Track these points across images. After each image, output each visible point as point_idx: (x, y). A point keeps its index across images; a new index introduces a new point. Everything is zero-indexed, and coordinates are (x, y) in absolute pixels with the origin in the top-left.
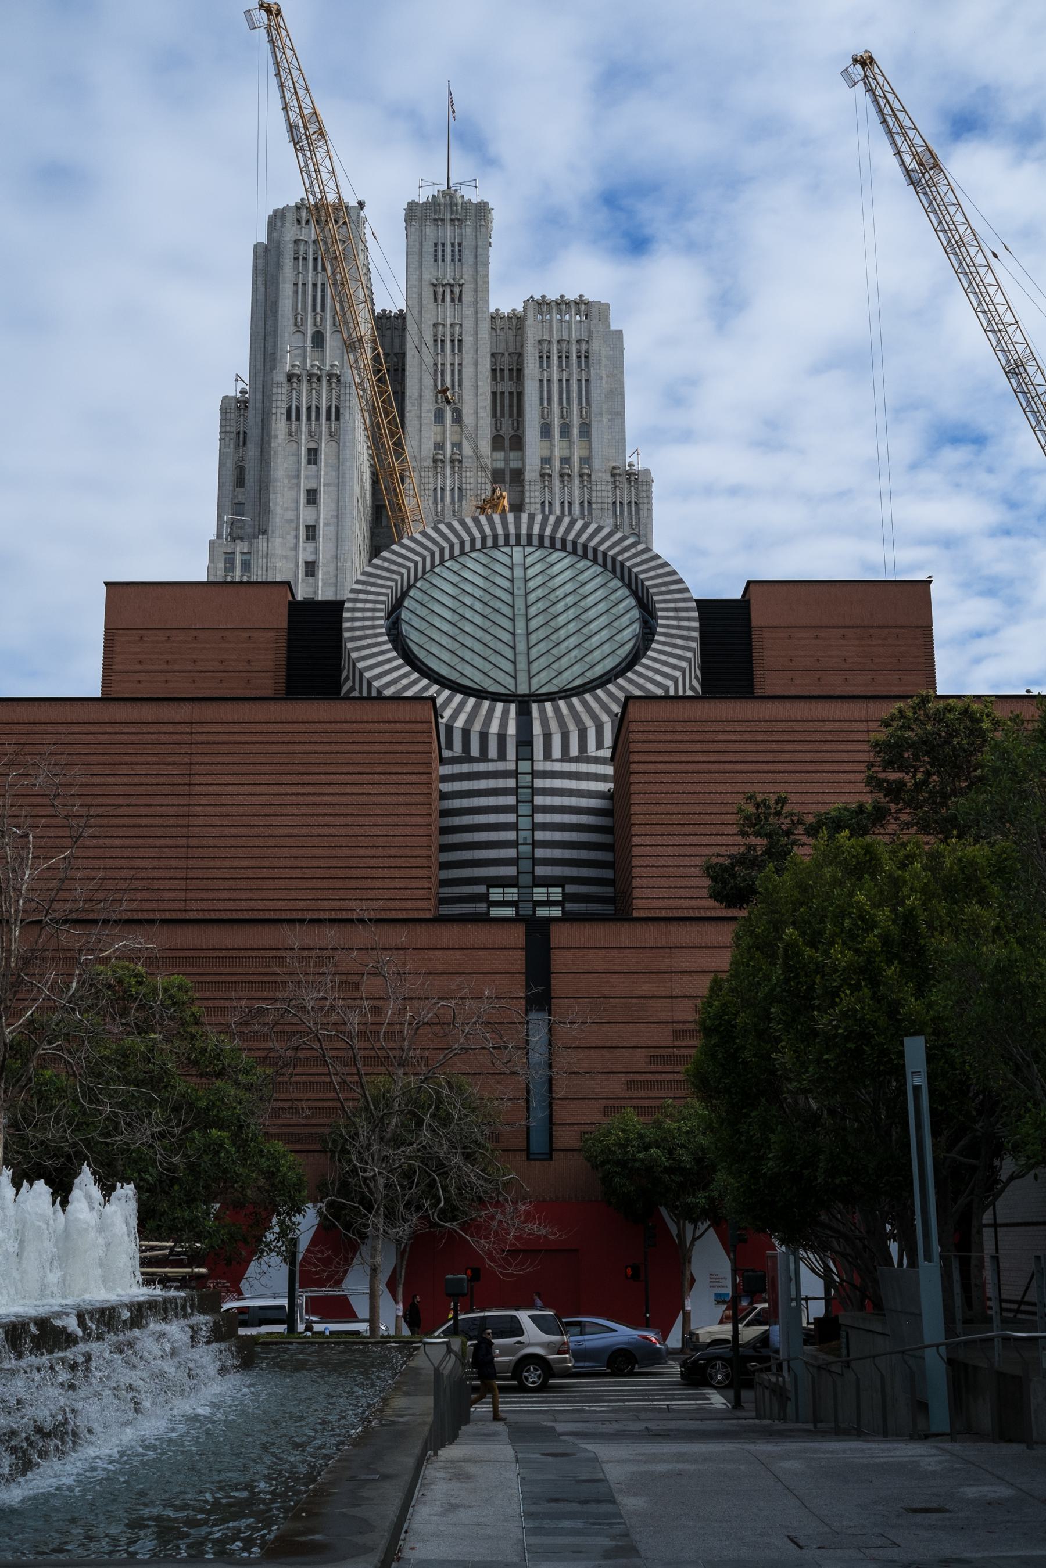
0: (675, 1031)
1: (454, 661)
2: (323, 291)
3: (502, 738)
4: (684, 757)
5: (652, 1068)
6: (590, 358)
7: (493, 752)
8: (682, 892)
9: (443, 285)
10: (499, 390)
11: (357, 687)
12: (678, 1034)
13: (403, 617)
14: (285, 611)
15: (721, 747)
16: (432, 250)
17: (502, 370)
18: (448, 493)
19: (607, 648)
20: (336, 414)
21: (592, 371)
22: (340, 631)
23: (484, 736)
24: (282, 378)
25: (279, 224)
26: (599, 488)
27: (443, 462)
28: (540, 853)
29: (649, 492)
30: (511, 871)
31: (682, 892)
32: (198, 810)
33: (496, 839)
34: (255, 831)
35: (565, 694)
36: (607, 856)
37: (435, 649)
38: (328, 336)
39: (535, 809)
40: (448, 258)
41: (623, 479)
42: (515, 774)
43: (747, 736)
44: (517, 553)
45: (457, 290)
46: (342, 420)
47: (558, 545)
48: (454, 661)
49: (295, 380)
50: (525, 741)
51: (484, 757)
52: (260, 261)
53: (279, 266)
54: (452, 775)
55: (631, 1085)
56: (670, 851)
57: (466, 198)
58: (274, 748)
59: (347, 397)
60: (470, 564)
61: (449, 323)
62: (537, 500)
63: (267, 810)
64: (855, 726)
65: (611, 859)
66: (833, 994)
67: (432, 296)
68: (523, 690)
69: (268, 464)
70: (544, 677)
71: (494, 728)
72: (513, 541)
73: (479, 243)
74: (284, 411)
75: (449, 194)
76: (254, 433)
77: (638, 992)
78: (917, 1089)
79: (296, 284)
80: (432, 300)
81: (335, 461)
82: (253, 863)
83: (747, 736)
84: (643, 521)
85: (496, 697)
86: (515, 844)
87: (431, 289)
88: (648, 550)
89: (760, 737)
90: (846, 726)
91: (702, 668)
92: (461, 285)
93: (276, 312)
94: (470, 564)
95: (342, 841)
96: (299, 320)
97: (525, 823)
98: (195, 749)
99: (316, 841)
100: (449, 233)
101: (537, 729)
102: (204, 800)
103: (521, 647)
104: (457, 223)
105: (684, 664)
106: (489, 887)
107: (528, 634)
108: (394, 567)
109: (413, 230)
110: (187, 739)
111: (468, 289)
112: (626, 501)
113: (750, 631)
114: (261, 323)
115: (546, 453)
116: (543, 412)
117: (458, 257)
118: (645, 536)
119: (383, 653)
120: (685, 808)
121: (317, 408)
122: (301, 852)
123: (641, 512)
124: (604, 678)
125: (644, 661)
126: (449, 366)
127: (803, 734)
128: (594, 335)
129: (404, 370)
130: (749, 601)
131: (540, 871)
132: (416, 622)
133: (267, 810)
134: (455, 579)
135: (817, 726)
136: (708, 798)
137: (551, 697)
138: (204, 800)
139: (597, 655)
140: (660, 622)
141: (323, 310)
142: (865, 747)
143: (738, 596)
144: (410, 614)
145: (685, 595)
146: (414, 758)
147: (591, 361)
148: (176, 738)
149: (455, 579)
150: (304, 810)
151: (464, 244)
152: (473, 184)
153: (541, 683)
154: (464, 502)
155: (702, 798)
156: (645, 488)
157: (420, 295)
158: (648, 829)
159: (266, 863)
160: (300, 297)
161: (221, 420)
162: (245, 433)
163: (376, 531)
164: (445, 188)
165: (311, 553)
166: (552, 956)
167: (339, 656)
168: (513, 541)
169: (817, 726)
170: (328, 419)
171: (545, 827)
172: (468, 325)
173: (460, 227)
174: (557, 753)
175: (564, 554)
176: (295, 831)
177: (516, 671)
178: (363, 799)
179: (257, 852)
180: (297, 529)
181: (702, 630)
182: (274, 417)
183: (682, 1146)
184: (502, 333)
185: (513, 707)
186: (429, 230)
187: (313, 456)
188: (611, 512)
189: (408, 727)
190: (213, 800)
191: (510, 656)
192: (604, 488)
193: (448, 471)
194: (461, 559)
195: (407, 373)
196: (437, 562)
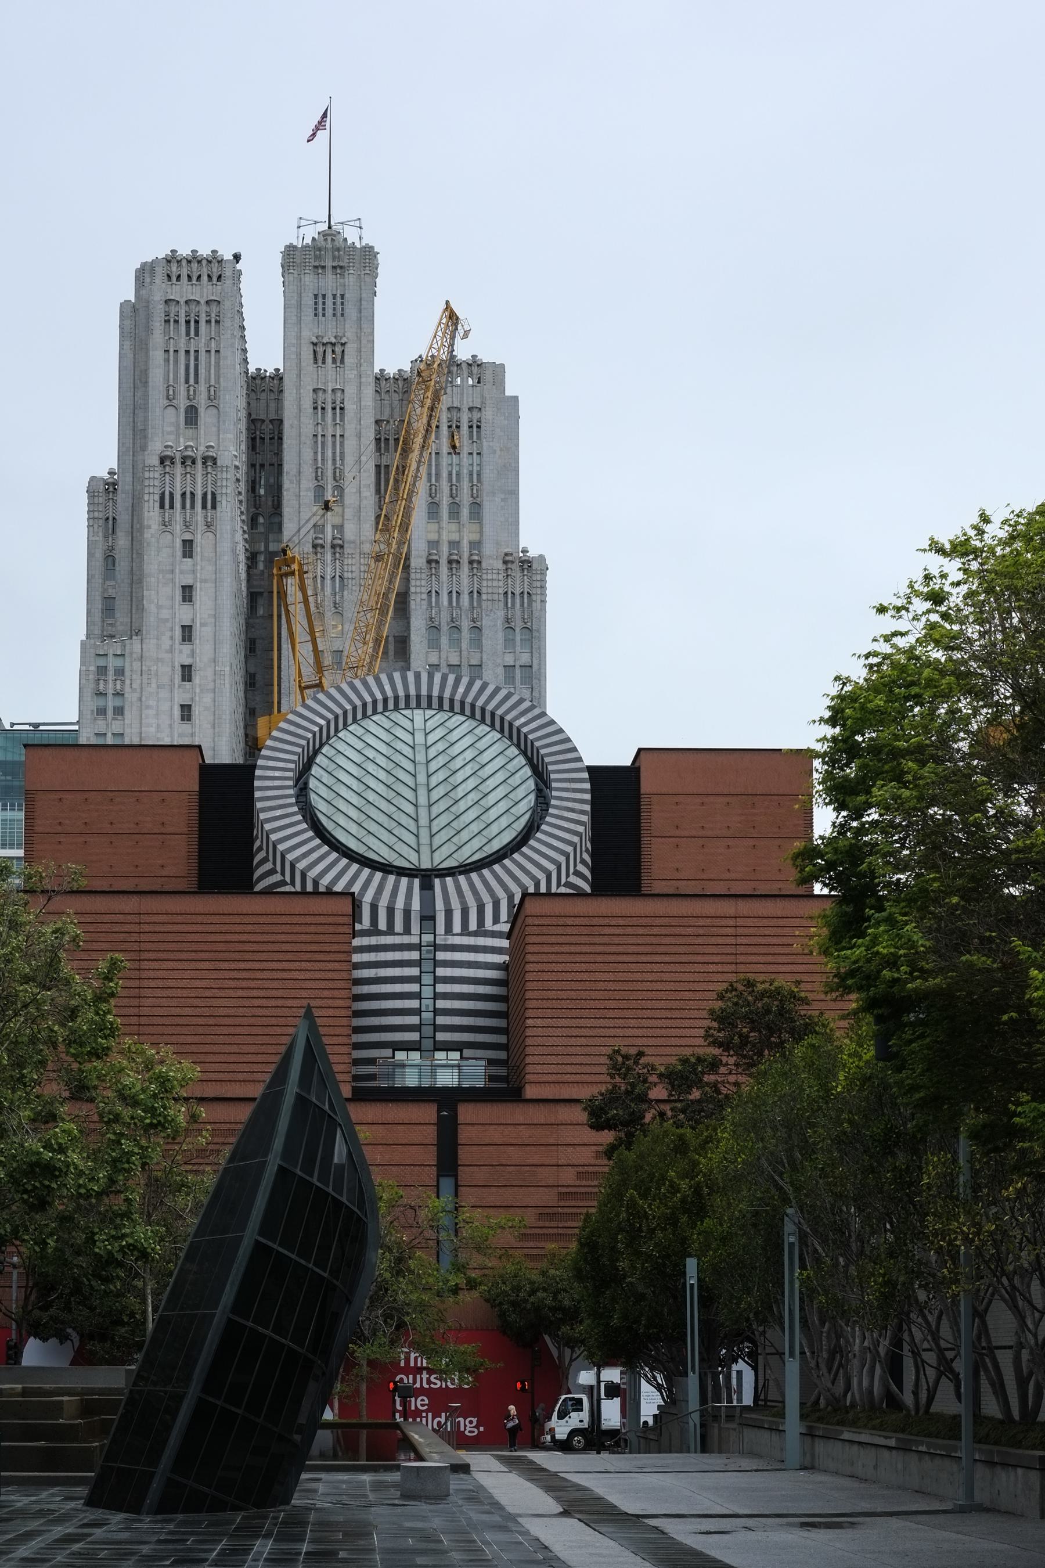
0: (560, 1194)
1: (361, 833)
2: (196, 359)
3: (407, 913)
4: (573, 949)
5: (541, 1223)
6: (483, 428)
7: (399, 927)
8: (569, 1069)
9: (324, 344)
10: (384, 463)
11: (271, 858)
12: (562, 1196)
13: (311, 785)
14: (196, 774)
15: (606, 940)
16: (311, 302)
17: (387, 440)
18: (328, 582)
19: (504, 822)
20: (211, 502)
21: (485, 443)
23: (391, 911)
24: (156, 461)
25: (148, 280)
26: (490, 577)
27: (323, 547)
28: (441, 1020)
29: (543, 581)
30: (414, 1036)
31: (569, 1069)
32: (147, 992)
33: (401, 1007)
34: (198, 1012)
35: (465, 869)
36: (502, 1039)
37: (342, 820)
38: (202, 411)
39: (437, 980)
40: (329, 312)
41: (515, 567)
42: (418, 947)
43: (629, 930)
44: (418, 715)
45: (338, 349)
46: (218, 509)
47: (457, 709)
48: (361, 833)
49: (168, 463)
50: (428, 918)
51: (390, 931)
52: (127, 322)
53: (149, 330)
54: (362, 946)
55: (524, 1237)
56: (558, 1032)
57: (349, 242)
58: (212, 937)
59: (224, 484)
60: (373, 728)
61: (330, 389)
62: (424, 590)
63: (208, 993)
64: (724, 922)
65: (505, 1041)
66: (652, 1231)
67: (312, 356)
68: (426, 865)
69: (140, 555)
70: (445, 851)
71: (400, 904)
72: (413, 704)
73: (364, 295)
74: (157, 498)
75: (330, 234)
76: (124, 519)
77: (530, 1161)
78: (692, 1285)
79: (167, 351)
80: (312, 361)
81: (213, 554)
82: (196, 1039)
83: (629, 930)
84: (536, 614)
85: (401, 872)
86: (418, 1012)
87: (311, 347)
88: (543, 714)
89: (641, 931)
90: (717, 922)
91: (593, 841)
92: (343, 344)
93: (146, 382)
94: (373, 728)
95: (274, 1021)
96: (171, 392)
97: (427, 992)
98: (143, 937)
99: (252, 1021)
100: (329, 283)
101: (440, 905)
102: (153, 984)
103: (424, 821)
104: (339, 271)
105: (576, 839)
106: (394, 1050)
107: (430, 806)
108: (300, 732)
109: (291, 279)
110: (136, 928)
111: (350, 349)
112: (517, 592)
113: (639, 798)
114: (130, 394)
115: (434, 537)
116: (431, 489)
117: (339, 313)
118: (538, 631)
120: (573, 995)
121: (192, 494)
122: (238, 1030)
123: (534, 604)
124: (501, 852)
125: (539, 835)
126: (330, 438)
127: (678, 929)
128: (488, 402)
129: (281, 439)
130: (639, 768)
131: (441, 1036)
132: (323, 791)
133: (208, 993)
134: (359, 745)
135: (692, 921)
136: (593, 986)
137: (451, 872)
138: (153, 984)
139: (494, 829)
140: (554, 793)
141: (197, 382)
142: (705, 1014)
143: (627, 762)
144: (317, 782)
145: (578, 765)
146: (335, 948)
147: (483, 433)
148: (127, 928)
149: (359, 745)
150: (240, 993)
151: (347, 296)
152: (357, 223)
153: (442, 858)
154: (345, 593)
155: (587, 985)
156: (538, 584)
157: (299, 355)
158: (540, 1013)
159: (208, 1039)
160: (171, 366)
161: (89, 504)
162: (114, 518)
163: (251, 621)
164: (325, 227)
165: (188, 656)
166: (459, 1131)
167: (251, 826)
168: (413, 704)
169: (692, 921)
170: (204, 507)
171: (446, 996)
172: (351, 391)
173: (342, 275)
174: (457, 928)
175: (463, 718)
176: (232, 1012)
177: (419, 845)
178: (290, 984)
179: (200, 1030)
180: (172, 629)
181: (593, 803)
182: (146, 504)
183: (565, 1290)
184: (387, 397)
185: (417, 882)
186: (309, 279)
187: (188, 549)
188: (502, 604)
189: (331, 920)
190: (160, 983)
191: (413, 829)
192: (495, 577)
193: (329, 557)
194: (364, 723)
195: (285, 446)
196: (341, 726)
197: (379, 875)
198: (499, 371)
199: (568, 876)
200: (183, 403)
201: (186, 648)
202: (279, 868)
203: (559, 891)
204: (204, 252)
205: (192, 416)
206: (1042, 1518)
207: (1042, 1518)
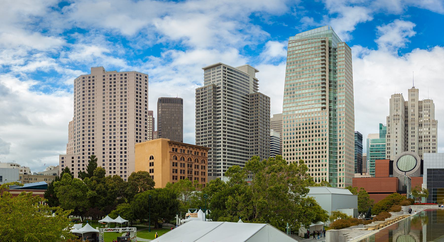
20: (399, 119)
22: (393, 166)
80: (388, 172)
100: (413, 93)
137: (408, 171)
187: (397, 124)
198: (432, 101)
200: (396, 109)
201: (397, 134)
204: (398, 94)
205: (397, 110)
206: (1, 177)
207: (1, 177)
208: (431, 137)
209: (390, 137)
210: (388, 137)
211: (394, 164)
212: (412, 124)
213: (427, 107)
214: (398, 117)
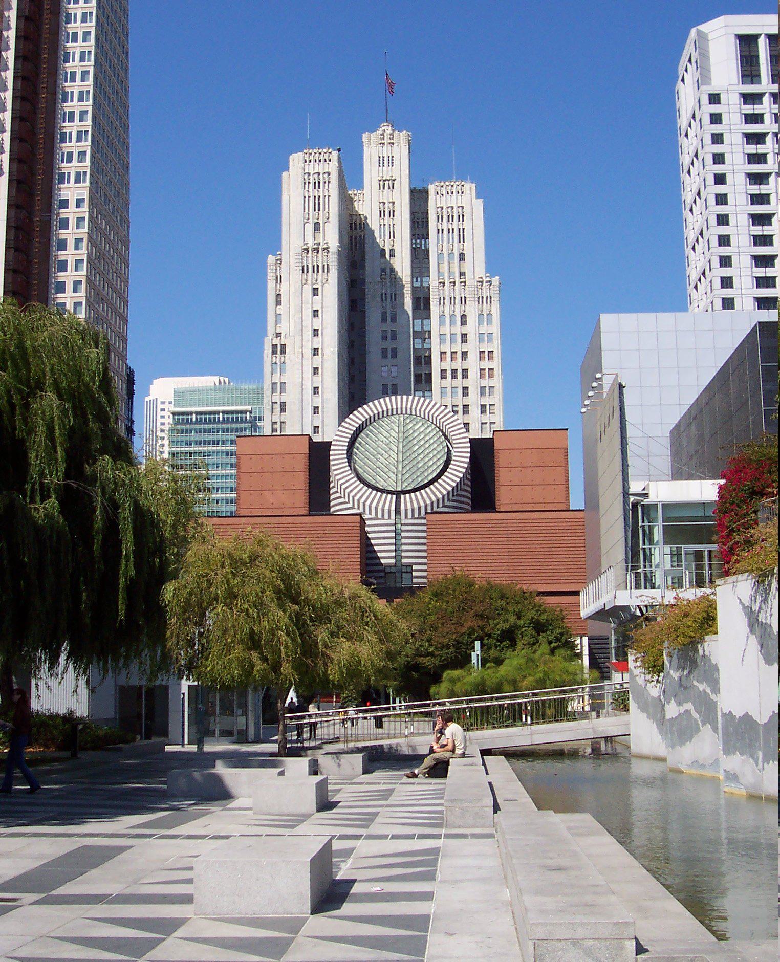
2: (319, 199)
3: (389, 511)
7: (386, 516)
22: (329, 461)
23: (383, 510)
50: (398, 511)
51: (383, 518)
68: (399, 489)
71: (387, 507)
85: (389, 492)
119: (346, 471)
137: (409, 492)
185: (394, 496)
197: (379, 494)
199: (457, 491)
202: (339, 491)
203: (438, 510)
208: (473, 356)
209: (283, 352)
210: (274, 352)
211: (337, 457)
212: (383, 298)
213: (450, 218)
214: (320, 260)
